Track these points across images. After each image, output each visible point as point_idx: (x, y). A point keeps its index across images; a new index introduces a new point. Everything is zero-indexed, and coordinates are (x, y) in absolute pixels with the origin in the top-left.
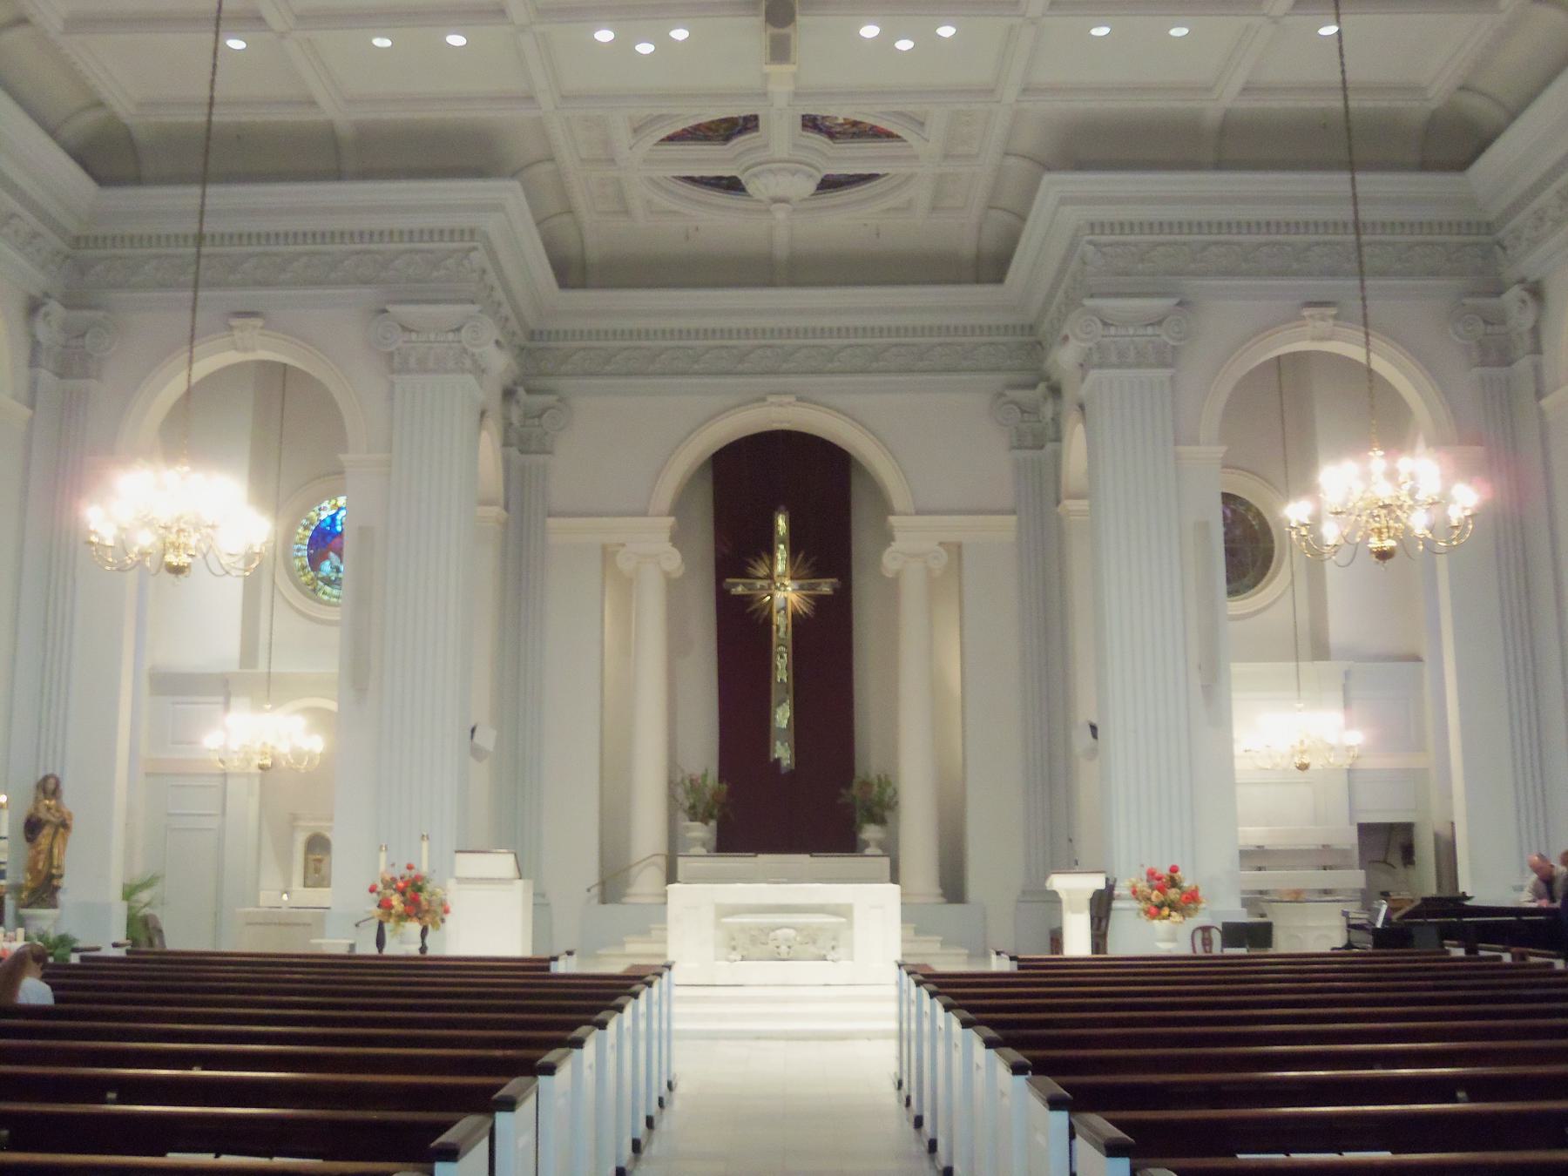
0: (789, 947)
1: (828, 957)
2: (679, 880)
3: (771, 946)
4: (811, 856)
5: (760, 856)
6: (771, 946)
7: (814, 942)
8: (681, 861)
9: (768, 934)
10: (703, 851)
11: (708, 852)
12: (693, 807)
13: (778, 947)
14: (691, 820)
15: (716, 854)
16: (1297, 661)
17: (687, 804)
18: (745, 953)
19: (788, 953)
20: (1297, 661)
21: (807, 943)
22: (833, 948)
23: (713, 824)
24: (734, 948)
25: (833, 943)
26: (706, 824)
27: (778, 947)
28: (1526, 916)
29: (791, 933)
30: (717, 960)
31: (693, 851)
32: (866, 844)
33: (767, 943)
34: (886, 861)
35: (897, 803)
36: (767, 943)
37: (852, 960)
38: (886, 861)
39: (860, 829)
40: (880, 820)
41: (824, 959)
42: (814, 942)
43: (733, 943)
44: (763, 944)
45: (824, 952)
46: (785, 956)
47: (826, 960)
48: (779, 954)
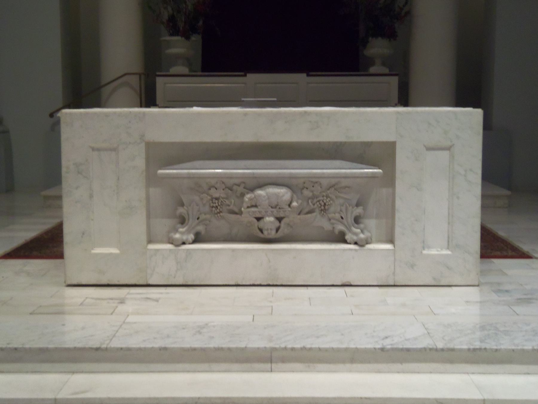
0: (280, 219)
1: (348, 237)
2: (157, 103)
3: (247, 217)
4: (308, 75)
5: (250, 76)
6: (247, 217)
7: (324, 209)
8: (160, 81)
9: (243, 195)
10: (184, 70)
11: (191, 70)
12: (172, 19)
13: (259, 219)
14: (172, 35)
15: (201, 73)
16: (271, 363)
17: (165, 16)
18: (201, 228)
19: (277, 230)
20: (271, 363)
21: (310, 212)
22: (357, 220)
23: (196, 39)
24: (183, 221)
25: (359, 211)
26: (188, 38)
27: (259, 219)
28: (274, 101)
29: (284, 193)
30: (150, 241)
31: (174, 70)
32: (370, 62)
33: (240, 213)
34: (394, 81)
35: (408, 13)
36: (240, 213)
37: (391, 241)
38: (394, 81)
39: (365, 44)
40: (391, 35)
41: (341, 239)
42: (324, 209)
43: (181, 210)
44: (233, 212)
45: (340, 227)
46: (273, 234)
47: (345, 242)
48: (261, 230)
